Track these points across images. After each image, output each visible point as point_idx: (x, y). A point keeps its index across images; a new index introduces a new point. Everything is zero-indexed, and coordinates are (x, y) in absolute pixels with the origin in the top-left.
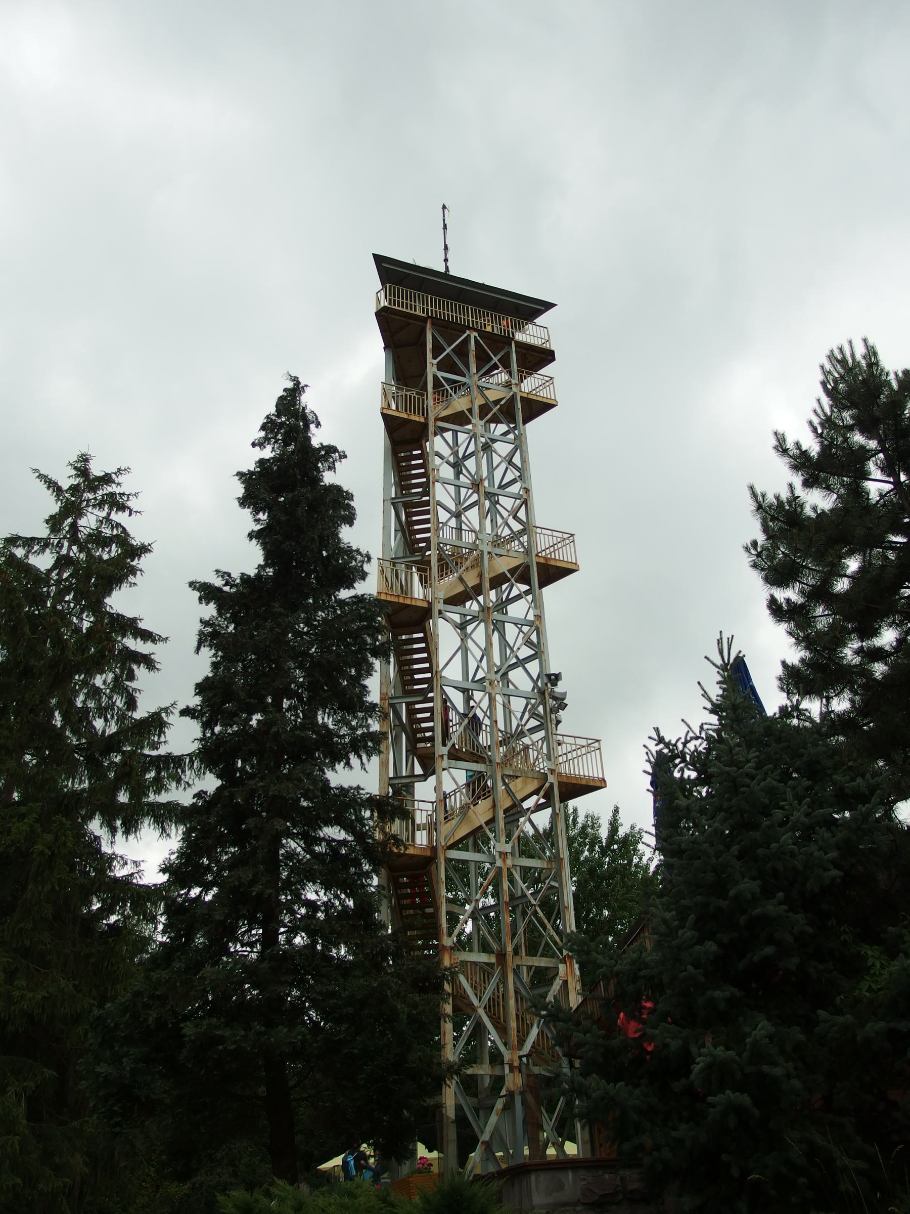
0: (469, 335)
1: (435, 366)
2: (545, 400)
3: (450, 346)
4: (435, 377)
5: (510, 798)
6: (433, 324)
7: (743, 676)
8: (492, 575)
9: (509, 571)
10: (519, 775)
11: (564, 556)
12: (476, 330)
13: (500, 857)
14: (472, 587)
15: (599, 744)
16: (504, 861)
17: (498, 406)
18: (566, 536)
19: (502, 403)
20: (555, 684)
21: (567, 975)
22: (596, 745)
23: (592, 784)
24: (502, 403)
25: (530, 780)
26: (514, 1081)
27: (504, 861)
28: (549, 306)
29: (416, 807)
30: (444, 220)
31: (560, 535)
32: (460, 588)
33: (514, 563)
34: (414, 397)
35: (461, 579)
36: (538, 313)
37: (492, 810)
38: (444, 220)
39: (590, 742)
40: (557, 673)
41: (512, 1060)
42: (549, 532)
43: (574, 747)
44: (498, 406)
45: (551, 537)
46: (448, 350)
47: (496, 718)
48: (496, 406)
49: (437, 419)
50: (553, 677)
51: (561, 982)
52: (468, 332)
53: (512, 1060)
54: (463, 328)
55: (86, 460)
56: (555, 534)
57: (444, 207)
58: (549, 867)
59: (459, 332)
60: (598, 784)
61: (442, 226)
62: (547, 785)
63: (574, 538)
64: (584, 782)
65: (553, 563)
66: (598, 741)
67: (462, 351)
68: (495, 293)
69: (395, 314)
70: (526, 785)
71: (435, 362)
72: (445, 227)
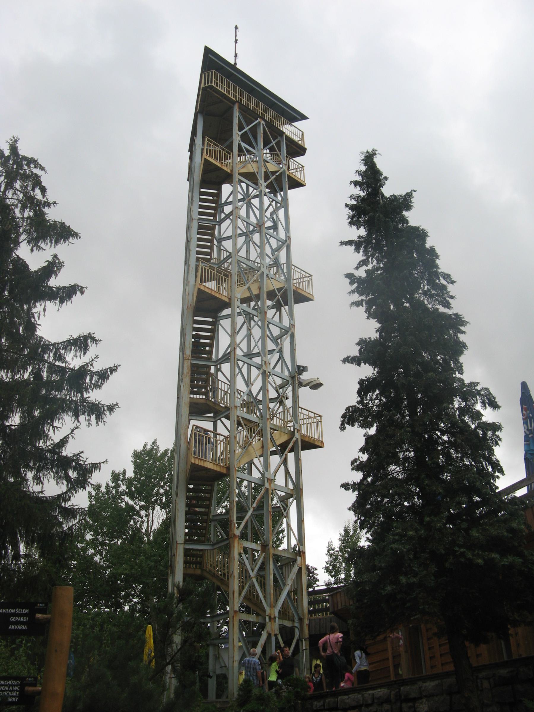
0: (259, 123)
1: (240, 136)
2: (299, 180)
3: (248, 126)
4: (240, 146)
5: (272, 443)
6: (239, 108)
7: (206, 444)
8: (268, 290)
9: (277, 289)
10: (277, 429)
11: (305, 288)
12: (264, 119)
13: (268, 482)
14: (255, 295)
15: (321, 419)
16: (270, 484)
17: (275, 176)
18: (307, 275)
19: (277, 174)
20: (301, 373)
21: (301, 564)
22: (319, 418)
23: (316, 443)
24: (277, 174)
25: (283, 434)
26: (271, 627)
27: (270, 484)
28: (304, 117)
29: (218, 438)
30: (236, 36)
31: (304, 273)
32: (247, 294)
33: (279, 285)
34: (225, 154)
35: (249, 289)
36: (296, 120)
37: (261, 449)
38: (236, 36)
39: (316, 415)
40: (304, 366)
41: (270, 614)
42: (299, 270)
43: (307, 417)
44: (275, 176)
45: (299, 274)
46: (246, 129)
47: (268, 388)
48: (273, 175)
49: (240, 174)
50: (302, 368)
51: (298, 568)
52: (259, 120)
53: (270, 614)
54: (257, 116)
55: (16, 141)
56: (302, 272)
57: (236, 27)
58: (292, 493)
59: (254, 118)
60: (320, 444)
61: (234, 40)
62: (294, 439)
63: (312, 278)
64: (311, 441)
65: (300, 291)
66: (320, 416)
67: (254, 131)
68: (273, 98)
69: (216, 92)
70: (281, 437)
71: (240, 133)
72: (236, 41)
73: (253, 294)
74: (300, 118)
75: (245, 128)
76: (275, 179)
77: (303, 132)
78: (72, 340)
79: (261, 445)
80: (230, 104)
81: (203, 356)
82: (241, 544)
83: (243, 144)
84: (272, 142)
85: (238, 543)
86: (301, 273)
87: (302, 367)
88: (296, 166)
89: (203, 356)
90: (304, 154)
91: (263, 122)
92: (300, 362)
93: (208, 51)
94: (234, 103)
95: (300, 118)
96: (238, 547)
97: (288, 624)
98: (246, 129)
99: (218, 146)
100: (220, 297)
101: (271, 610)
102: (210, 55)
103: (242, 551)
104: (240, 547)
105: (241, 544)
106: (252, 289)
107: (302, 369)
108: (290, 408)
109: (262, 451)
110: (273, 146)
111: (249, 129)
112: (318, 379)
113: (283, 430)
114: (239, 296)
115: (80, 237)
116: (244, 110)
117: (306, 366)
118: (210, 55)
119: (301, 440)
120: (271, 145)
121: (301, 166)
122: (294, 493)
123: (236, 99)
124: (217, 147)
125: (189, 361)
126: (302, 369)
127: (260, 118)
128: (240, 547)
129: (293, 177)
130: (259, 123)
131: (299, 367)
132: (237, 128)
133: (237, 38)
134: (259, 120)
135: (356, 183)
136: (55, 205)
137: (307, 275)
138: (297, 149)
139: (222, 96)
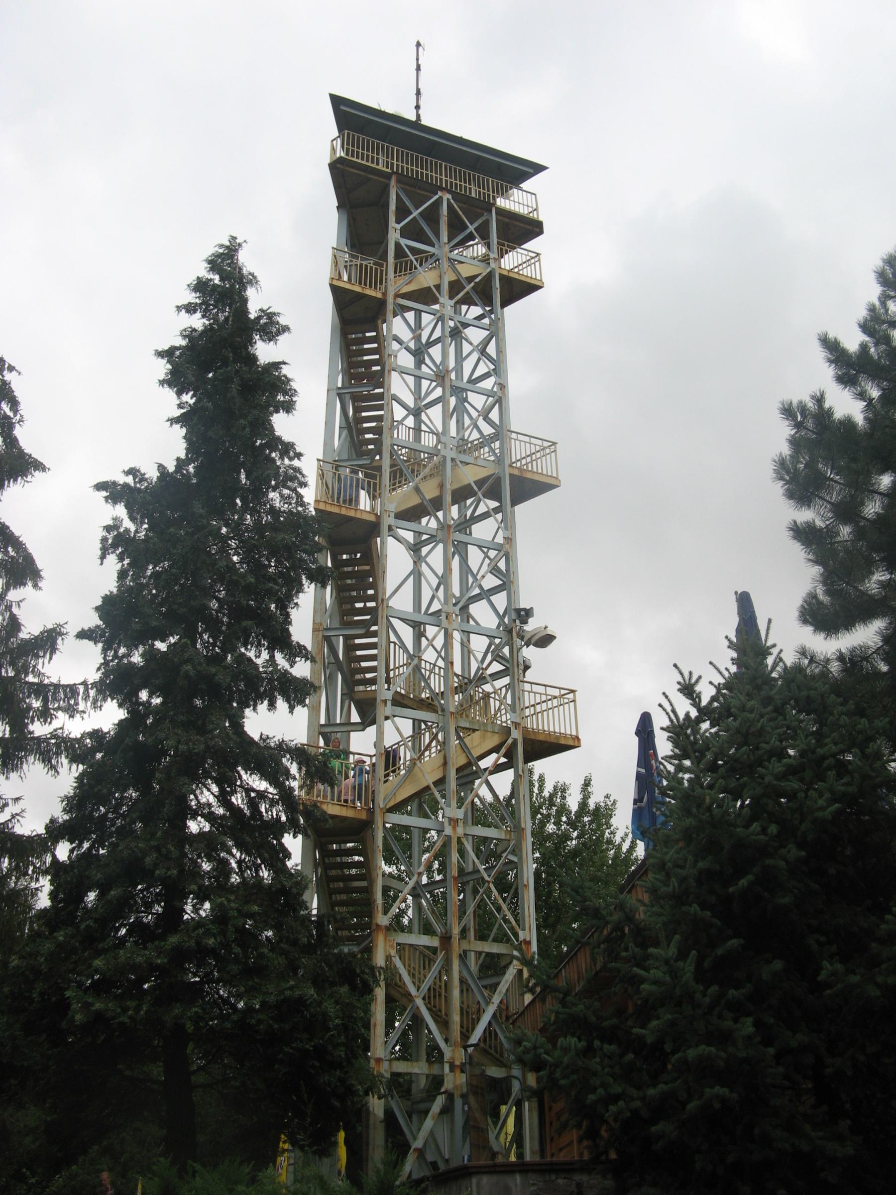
0: (441, 198)
1: (398, 232)
2: (529, 280)
3: (417, 209)
4: (398, 245)
5: (464, 754)
8: (456, 486)
9: (475, 482)
11: (543, 468)
12: (449, 192)
15: (574, 696)
17: (472, 284)
18: (546, 444)
19: (477, 280)
22: (571, 696)
23: (562, 742)
24: (477, 280)
25: (489, 734)
27: (454, 828)
28: (539, 168)
30: (417, 59)
31: (539, 442)
32: (415, 501)
33: (482, 473)
35: (417, 489)
36: (526, 176)
38: (417, 59)
39: (563, 692)
40: (528, 608)
41: (453, 1058)
42: (527, 439)
44: (472, 284)
45: (528, 445)
46: (415, 213)
48: (470, 283)
51: (515, 971)
52: (440, 193)
53: (453, 1058)
56: (533, 441)
57: (418, 44)
60: (571, 743)
62: (510, 741)
64: (553, 740)
66: (573, 691)
67: (431, 216)
69: (352, 167)
71: (399, 226)
72: (418, 68)
73: (425, 499)
74: (531, 171)
75: (411, 213)
76: (473, 288)
77: (534, 194)
78: (33, 639)
79: (442, 761)
80: (383, 180)
81: (356, 618)
82: (390, 941)
83: (404, 242)
84: (468, 227)
85: (385, 939)
86: (530, 443)
87: (524, 609)
88: (524, 257)
89: (356, 618)
90: (541, 232)
91: (447, 196)
92: (524, 604)
93: (337, 102)
94: (388, 176)
95: (531, 171)
96: (385, 946)
97: (495, 1072)
98: (415, 213)
99: (357, 258)
100: (358, 516)
101: (453, 1051)
102: (342, 107)
103: (393, 952)
104: (388, 945)
105: (390, 941)
106: (423, 490)
107: (525, 615)
108: (500, 689)
109: (444, 770)
110: (471, 232)
111: (420, 214)
112: (546, 628)
113: (489, 728)
114: (392, 507)
115: (49, 469)
116: (406, 181)
117: (532, 608)
118: (342, 107)
119: (524, 739)
120: (468, 231)
121: (534, 255)
122: (513, 838)
123: (392, 168)
124: (354, 260)
125: (321, 633)
126: (525, 615)
127: (442, 191)
128: (388, 945)
129: (516, 276)
130: (441, 198)
131: (518, 611)
132: (394, 219)
133: (420, 63)
134: (440, 193)
135: (190, 309)
136: (21, 423)
137: (546, 444)
138: (528, 227)
139: (365, 171)
